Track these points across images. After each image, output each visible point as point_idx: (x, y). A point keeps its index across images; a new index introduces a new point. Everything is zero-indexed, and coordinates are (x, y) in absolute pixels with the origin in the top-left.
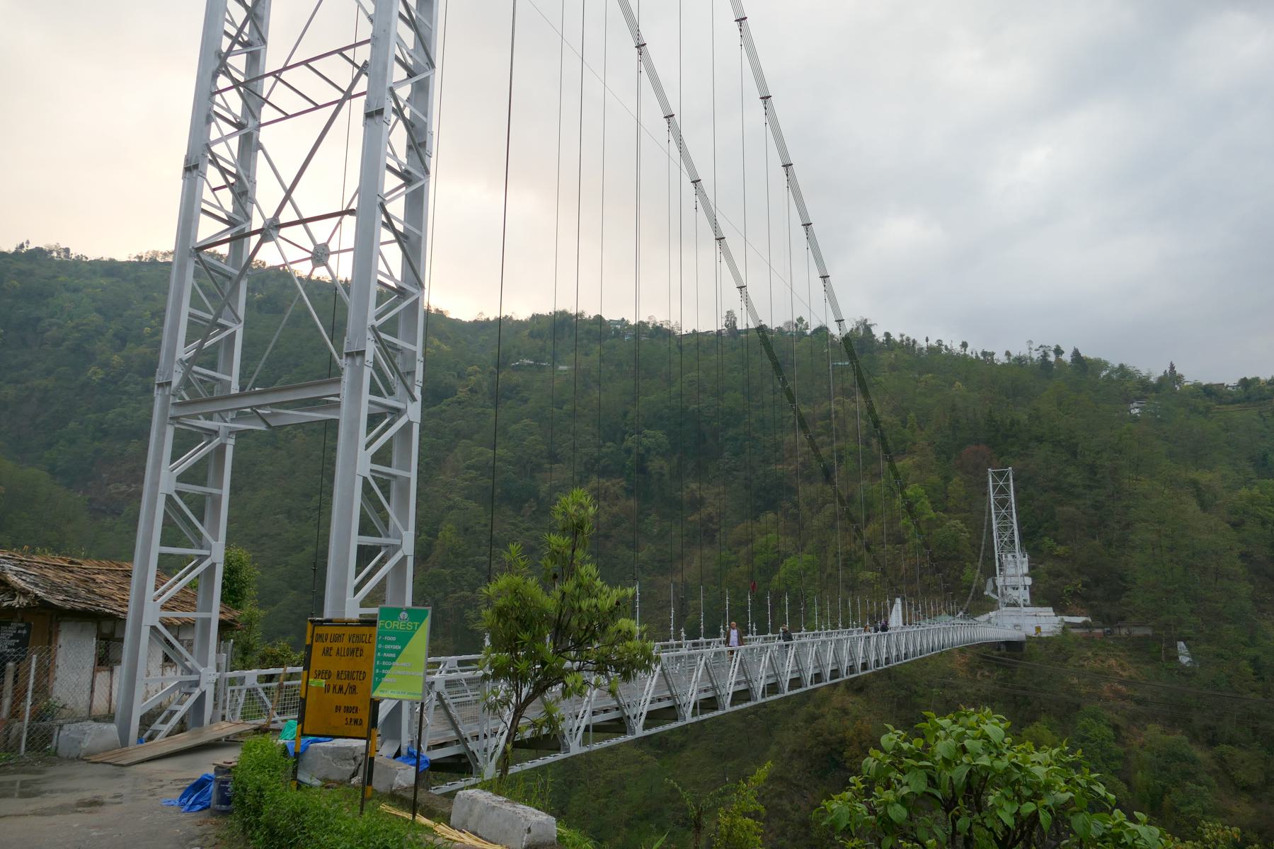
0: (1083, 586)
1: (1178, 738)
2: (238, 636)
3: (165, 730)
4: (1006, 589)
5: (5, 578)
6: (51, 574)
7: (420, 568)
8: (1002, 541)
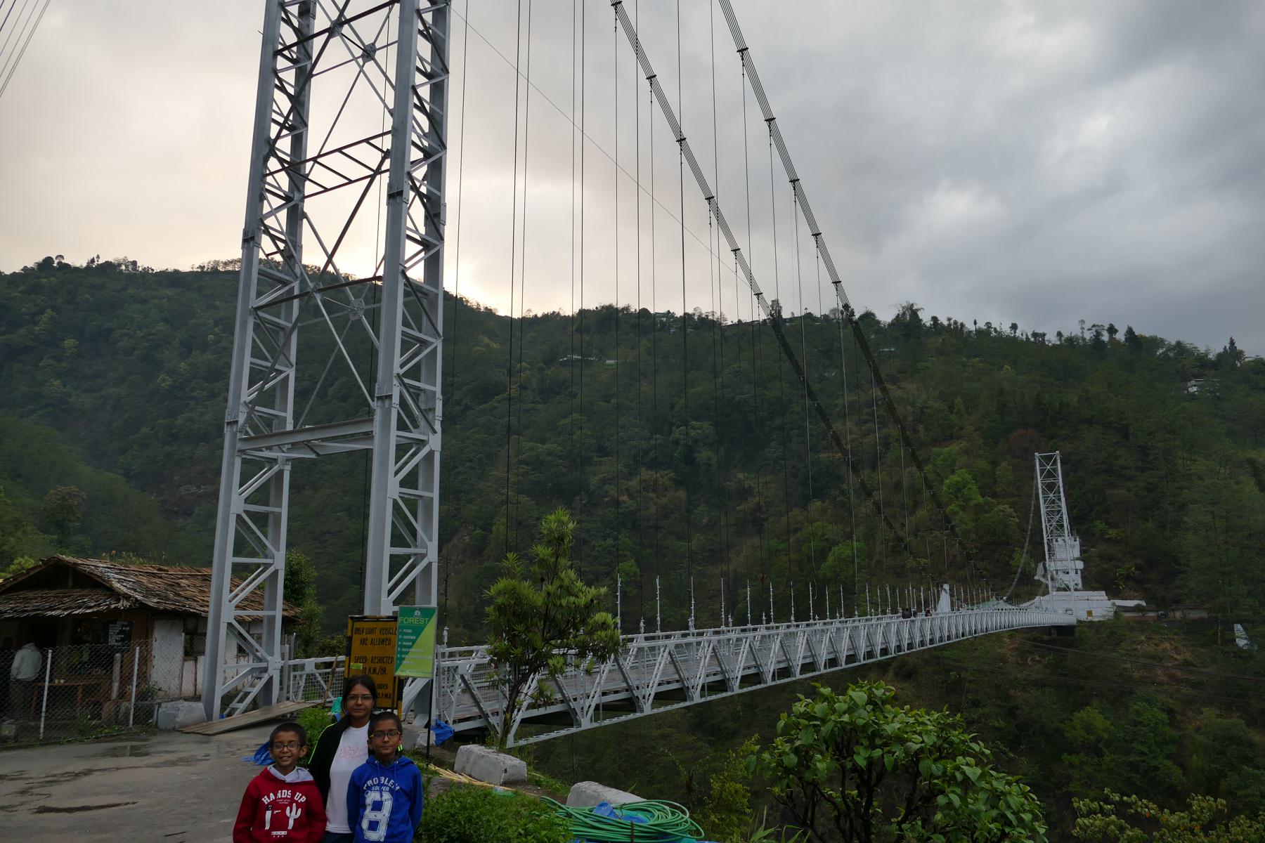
0: (1136, 570)
1: (1235, 722)
2: (300, 630)
3: (241, 708)
4: (1057, 574)
5: (111, 585)
6: (144, 580)
7: (476, 561)
8: (1051, 525)
